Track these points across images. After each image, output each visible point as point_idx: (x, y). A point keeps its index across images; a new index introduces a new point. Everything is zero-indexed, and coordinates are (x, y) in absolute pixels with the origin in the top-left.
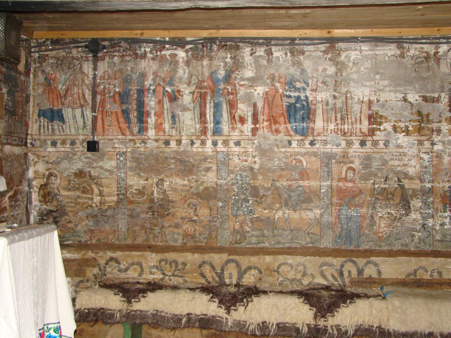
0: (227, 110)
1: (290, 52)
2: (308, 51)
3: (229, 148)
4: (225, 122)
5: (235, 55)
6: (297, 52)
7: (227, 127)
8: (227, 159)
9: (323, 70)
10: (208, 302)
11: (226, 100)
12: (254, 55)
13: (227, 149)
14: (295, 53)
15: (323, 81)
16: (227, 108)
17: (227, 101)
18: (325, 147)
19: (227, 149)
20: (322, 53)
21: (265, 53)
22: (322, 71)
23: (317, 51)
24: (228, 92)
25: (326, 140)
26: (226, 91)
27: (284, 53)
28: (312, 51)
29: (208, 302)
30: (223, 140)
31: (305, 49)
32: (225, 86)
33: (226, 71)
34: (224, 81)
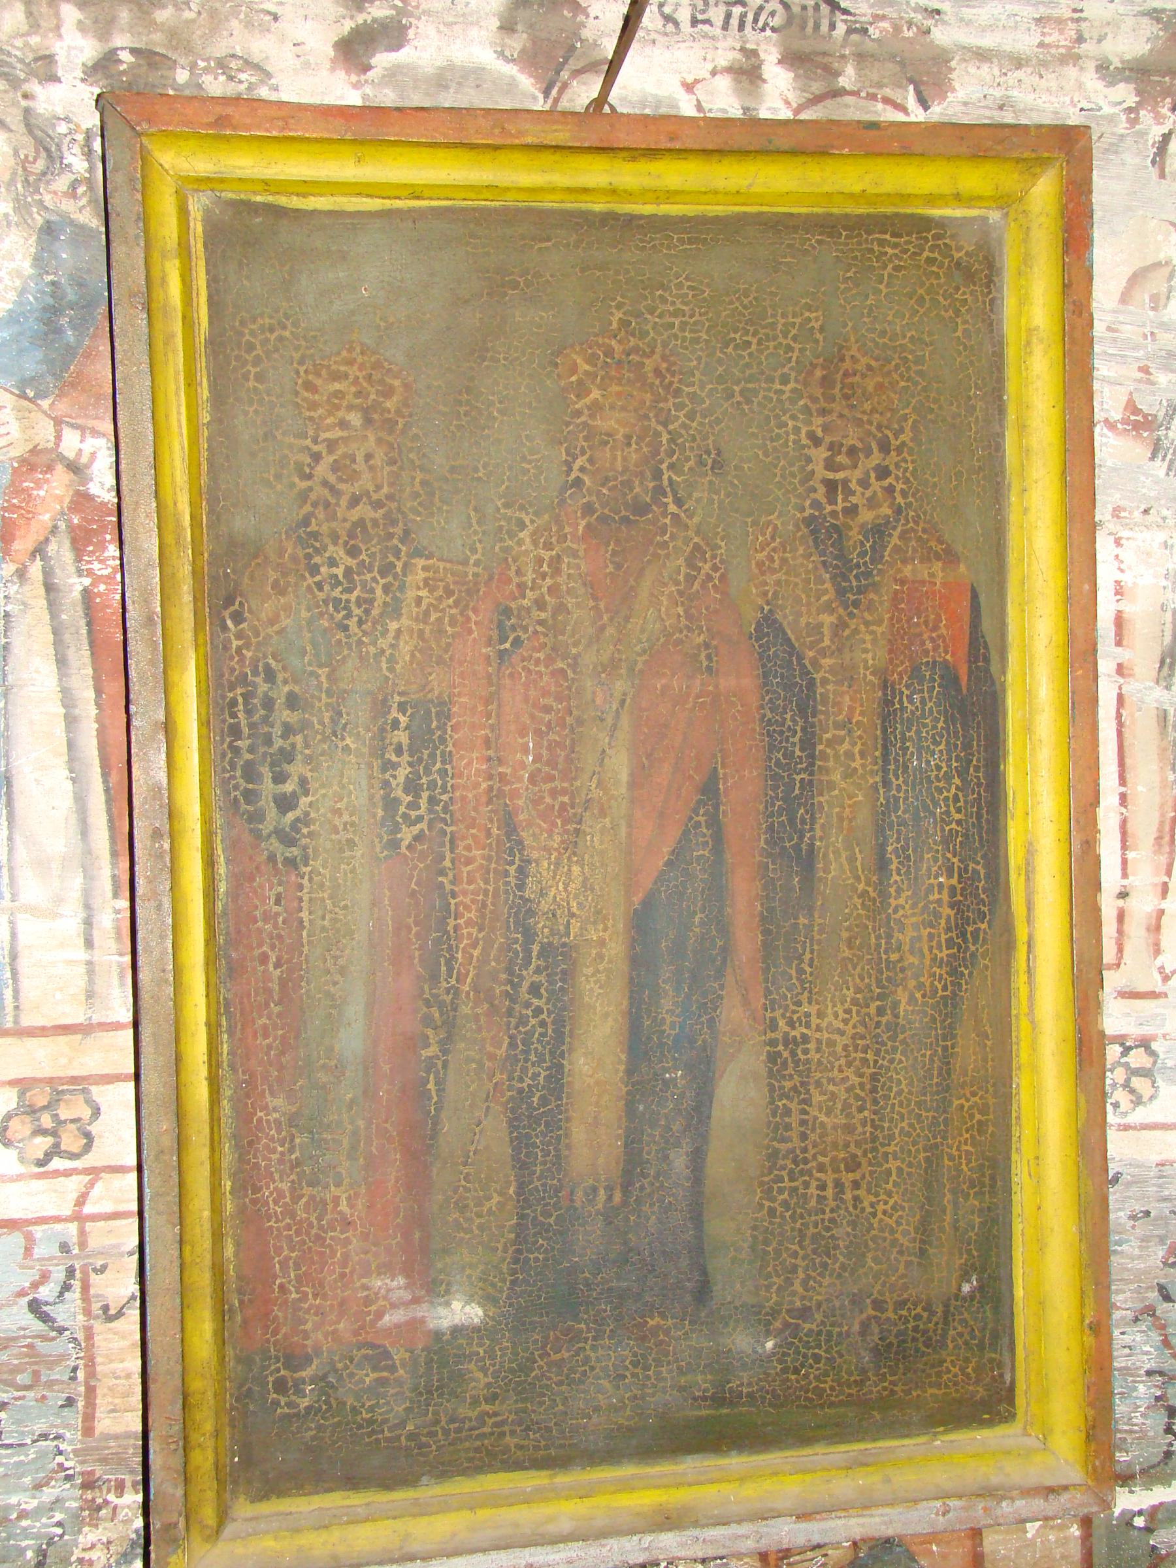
0: (71, 721)
1: (792, 59)
2: (982, 56)
3: (94, 1172)
4: (41, 865)
5: (157, 41)
6: (861, 57)
7: (72, 924)
8: (68, 1312)
9: (1136, 279)
10: (57, 80)
11: (53, 607)
12: (382, 60)
13: (74, 1185)
14: (848, 78)
15: (1132, 407)
16: (67, 698)
17: (73, 615)
18: (1139, 1116)
19: (74, 1185)
20: (1125, 93)
21: (517, 43)
22: (1125, 298)
23: (1071, 58)
24: (82, 500)
25: (1145, 1043)
26: (58, 485)
27: (726, 55)
28: (1019, 62)
29: (57, 80)
30: (23, 1085)
31: (942, 36)
32: (45, 432)
33: (49, 231)
34: (32, 364)
